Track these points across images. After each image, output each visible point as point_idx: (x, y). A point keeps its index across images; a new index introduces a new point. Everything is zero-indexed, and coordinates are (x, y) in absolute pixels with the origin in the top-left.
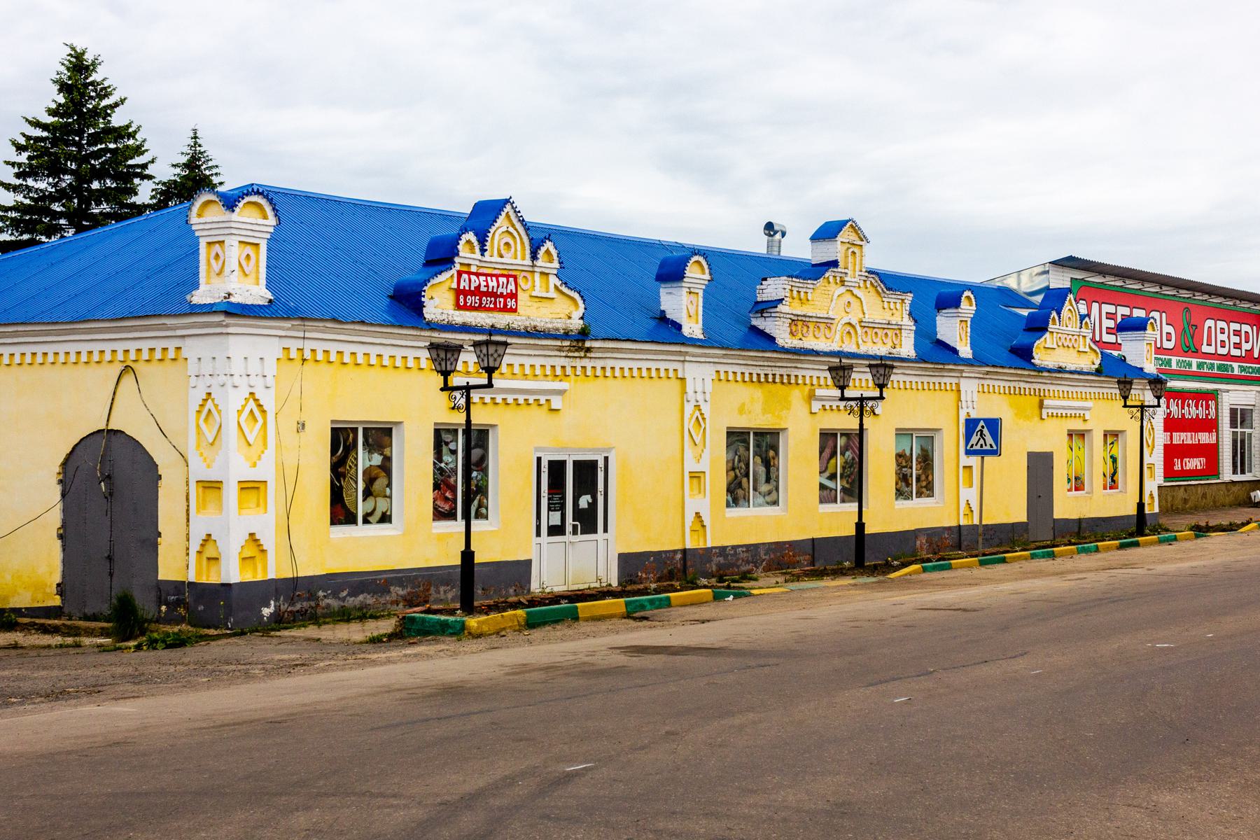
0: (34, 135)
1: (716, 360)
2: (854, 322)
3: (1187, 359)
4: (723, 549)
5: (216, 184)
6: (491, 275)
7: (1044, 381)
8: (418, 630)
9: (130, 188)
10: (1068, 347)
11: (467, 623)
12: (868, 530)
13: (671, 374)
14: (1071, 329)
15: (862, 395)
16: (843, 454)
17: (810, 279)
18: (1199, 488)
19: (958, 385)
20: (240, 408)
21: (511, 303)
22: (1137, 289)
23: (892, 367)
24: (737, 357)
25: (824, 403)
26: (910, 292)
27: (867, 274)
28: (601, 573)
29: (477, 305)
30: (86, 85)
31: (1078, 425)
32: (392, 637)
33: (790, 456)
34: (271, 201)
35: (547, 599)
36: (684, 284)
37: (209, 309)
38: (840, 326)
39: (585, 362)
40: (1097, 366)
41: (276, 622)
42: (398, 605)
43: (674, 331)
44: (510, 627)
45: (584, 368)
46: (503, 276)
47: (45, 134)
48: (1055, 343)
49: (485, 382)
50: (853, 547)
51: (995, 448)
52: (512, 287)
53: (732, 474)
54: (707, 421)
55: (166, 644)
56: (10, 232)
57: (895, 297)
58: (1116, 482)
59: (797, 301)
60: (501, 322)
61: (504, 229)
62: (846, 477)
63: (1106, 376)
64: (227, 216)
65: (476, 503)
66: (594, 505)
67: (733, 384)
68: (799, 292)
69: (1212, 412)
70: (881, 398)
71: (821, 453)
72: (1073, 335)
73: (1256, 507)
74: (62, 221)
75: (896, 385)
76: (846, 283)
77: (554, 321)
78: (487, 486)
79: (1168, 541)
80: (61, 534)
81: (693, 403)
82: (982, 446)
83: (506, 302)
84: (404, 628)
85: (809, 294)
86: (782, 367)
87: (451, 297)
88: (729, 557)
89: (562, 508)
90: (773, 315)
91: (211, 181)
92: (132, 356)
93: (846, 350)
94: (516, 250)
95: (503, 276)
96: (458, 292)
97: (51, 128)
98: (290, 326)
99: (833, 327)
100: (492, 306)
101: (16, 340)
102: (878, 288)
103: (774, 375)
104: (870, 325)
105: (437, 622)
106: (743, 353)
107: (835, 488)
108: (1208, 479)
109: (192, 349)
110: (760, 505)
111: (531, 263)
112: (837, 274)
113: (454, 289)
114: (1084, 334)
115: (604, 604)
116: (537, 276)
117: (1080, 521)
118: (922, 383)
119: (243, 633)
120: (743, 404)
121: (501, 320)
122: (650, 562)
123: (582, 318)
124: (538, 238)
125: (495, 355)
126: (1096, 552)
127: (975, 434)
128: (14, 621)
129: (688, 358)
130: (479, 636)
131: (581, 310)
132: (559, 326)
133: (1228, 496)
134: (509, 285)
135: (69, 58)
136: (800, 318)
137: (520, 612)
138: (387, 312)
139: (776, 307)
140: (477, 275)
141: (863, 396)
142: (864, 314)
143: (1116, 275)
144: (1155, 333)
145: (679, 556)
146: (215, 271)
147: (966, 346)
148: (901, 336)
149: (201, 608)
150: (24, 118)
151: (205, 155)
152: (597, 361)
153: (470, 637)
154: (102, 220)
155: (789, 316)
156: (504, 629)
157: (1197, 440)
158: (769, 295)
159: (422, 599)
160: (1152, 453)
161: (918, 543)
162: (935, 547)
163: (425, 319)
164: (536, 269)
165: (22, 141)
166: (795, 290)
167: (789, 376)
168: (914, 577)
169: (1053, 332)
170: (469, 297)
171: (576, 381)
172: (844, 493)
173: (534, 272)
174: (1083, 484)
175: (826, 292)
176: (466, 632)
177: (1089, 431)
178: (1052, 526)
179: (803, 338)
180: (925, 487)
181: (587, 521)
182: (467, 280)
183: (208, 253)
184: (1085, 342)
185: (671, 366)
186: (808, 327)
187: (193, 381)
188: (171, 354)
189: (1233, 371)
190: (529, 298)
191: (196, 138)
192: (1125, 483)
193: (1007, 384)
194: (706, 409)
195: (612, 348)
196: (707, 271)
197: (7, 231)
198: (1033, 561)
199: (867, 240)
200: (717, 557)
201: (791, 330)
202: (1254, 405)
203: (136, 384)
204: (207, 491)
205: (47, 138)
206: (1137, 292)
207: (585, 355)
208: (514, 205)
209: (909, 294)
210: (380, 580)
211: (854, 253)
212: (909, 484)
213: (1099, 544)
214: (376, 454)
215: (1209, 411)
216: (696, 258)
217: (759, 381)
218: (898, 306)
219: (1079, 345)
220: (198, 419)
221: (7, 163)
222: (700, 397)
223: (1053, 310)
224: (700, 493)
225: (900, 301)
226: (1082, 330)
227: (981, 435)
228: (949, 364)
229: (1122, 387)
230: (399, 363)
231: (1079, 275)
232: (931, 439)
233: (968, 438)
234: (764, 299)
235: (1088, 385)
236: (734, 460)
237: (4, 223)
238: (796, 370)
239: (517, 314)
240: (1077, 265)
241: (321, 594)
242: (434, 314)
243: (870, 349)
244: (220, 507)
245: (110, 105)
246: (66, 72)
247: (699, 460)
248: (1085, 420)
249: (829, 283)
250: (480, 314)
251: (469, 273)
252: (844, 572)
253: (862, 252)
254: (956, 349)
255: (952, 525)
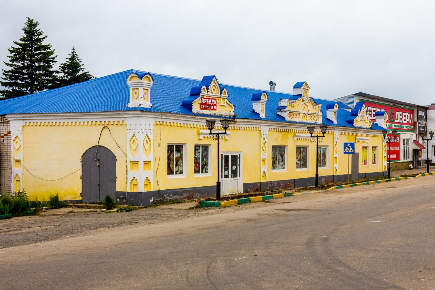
0: (16, 47)
1: (269, 125)
2: (306, 113)
3: (391, 124)
4: (271, 182)
5: (81, 65)
8: (205, 205)
9: (50, 66)
11: (221, 203)
12: (319, 176)
13: (257, 129)
16: (302, 153)
17: (294, 100)
19: (333, 132)
20: (144, 139)
21: (215, 107)
22: (378, 102)
25: (298, 138)
26: (321, 104)
27: (309, 98)
28: (238, 189)
29: (206, 108)
30: (34, 31)
31: (365, 145)
34: (152, 76)
36: (260, 102)
37: (135, 109)
38: (302, 114)
39: (235, 126)
40: (371, 126)
41: (154, 204)
42: (185, 199)
43: (257, 116)
45: (234, 127)
46: (213, 99)
47: (20, 47)
48: (359, 119)
49: (224, 132)
50: (216, 188)
51: (353, 151)
52: (215, 102)
55: (126, 210)
56: (8, 80)
57: (317, 105)
59: (291, 106)
61: (213, 85)
64: (140, 81)
66: (236, 169)
68: (291, 104)
69: (398, 140)
70: (324, 136)
73: (411, 170)
74: (26, 76)
76: (304, 101)
77: (226, 113)
80: (82, 178)
81: (263, 138)
82: (349, 151)
83: (213, 107)
84: (200, 205)
85: (294, 104)
87: (199, 105)
88: (273, 185)
89: (228, 170)
90: (284, 111)
91: (79, 64)
92: (107, 123)
93: (304, 121)
94: (216, 91)
95: (213, 99)
96: (201, 104)
97: (23, 45)
98: (157, 114)
99: (300, 114)
100: (210, 108)
101: (66, 118)
103: (284, 129)
104: (310, 114)
107: (300, 163)
108: (397, 161)
109: (128, 121)
110: (280, 169)
113: (200, 103)
114: (367, 117)
115: (257, 198)
116: (222, 99)
117: (366, 174)
119: (146, 207)
121: (213, 112)
123: (234, 112)
124: (222, 88)
125: (227, 124)
126: (380, 183)
127: (347, 147)
128: (67, 205)
129: (262, 124)
130: (225, 207)
131: (233, 110)
135: (28, 22)
136: (291, 112)
137: (236, 200)
138: (180, 109)
139: (285, 108)
141: (219, 132)
142: (308, 110)
144: (386, 116)
145: (259, 184)
146: (135, 98)
147: (335, 120)
149: (132, 200)
150: (13, 41)
151: (77, 55)
152: (238, 125)
153: (222, 207)
154: (40, 76)
155: (288, 111)
156: (232, 205)
163: (192, 112)
164: (222, 97)
165: (12, 49)
166: (290, 103)
167: (288, 129)
168: (334, 190)
170: (204, 105)
174: (366, 162)
176: (221, 206)
177: (368, 146)
179: (292, 118)
181: (235, 173)
182: (203, 100)
183: (133, 92)
184: (368, 119)
185: (257, 126)
186: (294, 114)
187: (128, 131)
188: (121, 123)
189: (404, 128)
191: (74, 50)
195: (242, 121)
196: (267, 97)
197: (8, 79)
201: (289, 115)
202: (410, 138)
203: (109, 132)
204: (133, 164)
205: (20, 48)
206: (377, 103)
207: (235, 123)
209: (321, 104)
210: (181, 191)
211: (306, 92)
213: (380, 180)
216: (264, 94)
217: (280, 131)
218: (318, 108)
220: (130, 143)
221: (8, 56)
223: (359, 109)
226: (367, 115)
227: (349, 148)
228: (331, 126)
229: (384, 133)
230: (185, 126)
231: (362, 98)
234: (281, 106)
236: (273, 155)
237: (6, 76)
241: (165, 195)
243: (310, 122)
244: (138, 169)
245: (42, 38)
246: (27, 27)
248: (367, 143)
249: (299, 101)
251: (204, 98)
252: (313, 189)
253: (308, 91)
255: (331, 175)
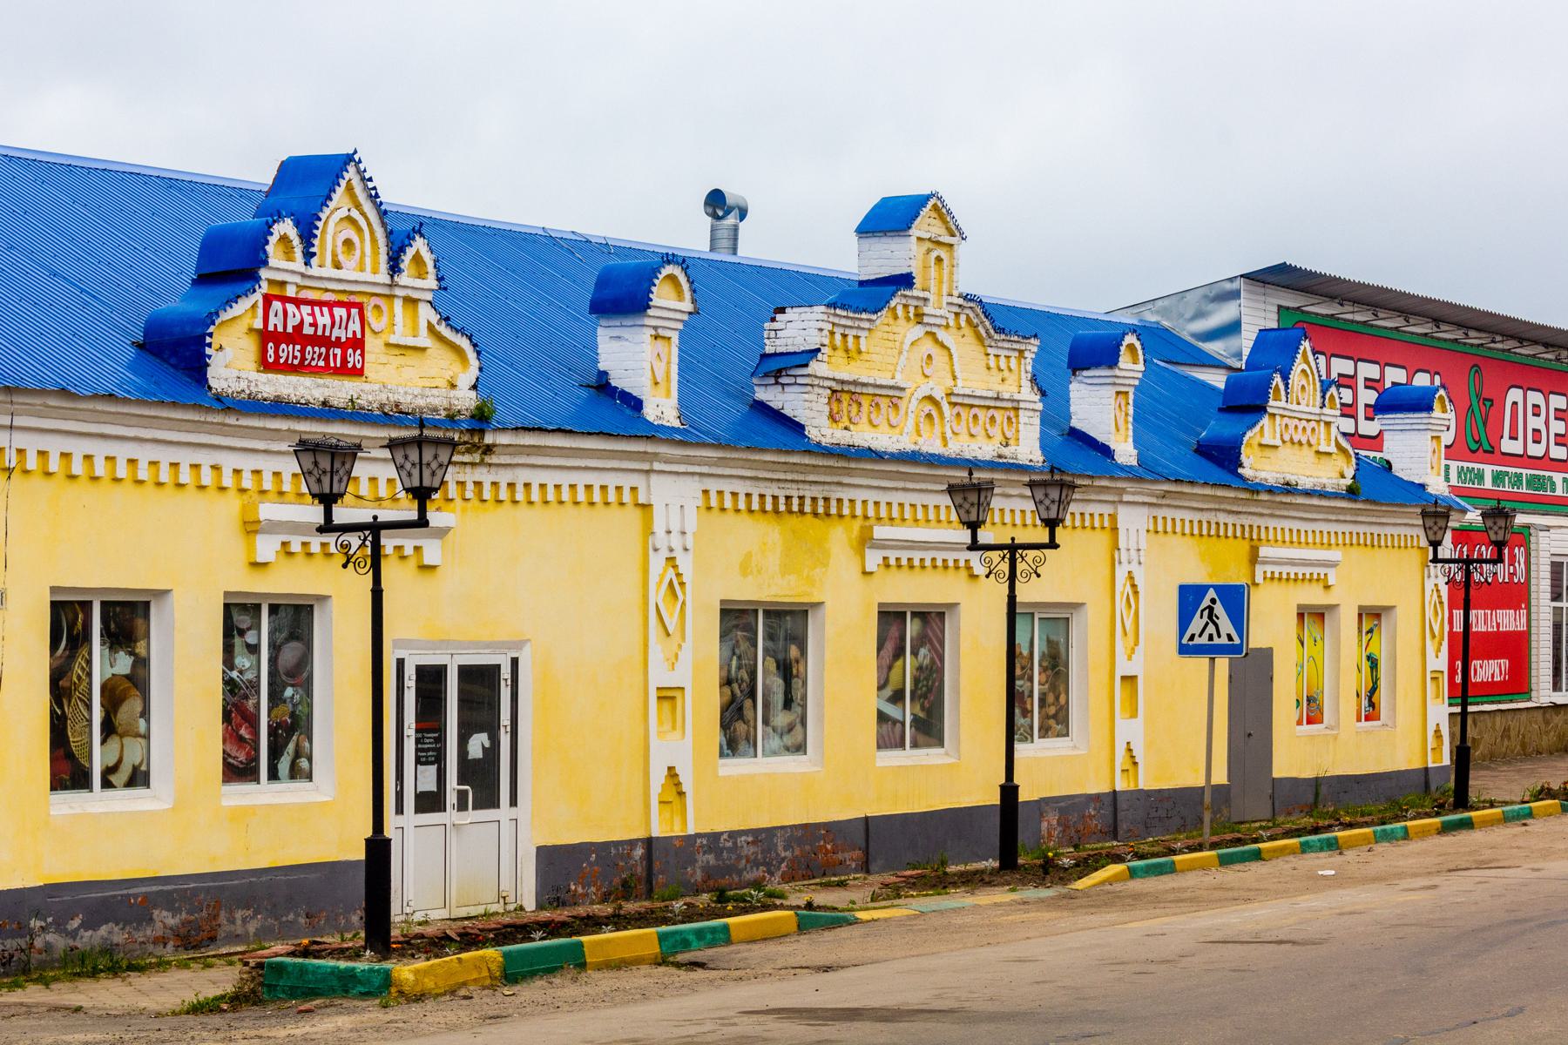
1: (705, 469)
2: (939, 394)
3: (1476, 466)
4: (714, 837)
6: (321, 304)
7: (1259, 510)
8: (292, 988)
10: (1300, 443)
11: (395, 974)
12: (1023, 796)
13: (627, 497)
14: (1307, 409)
15: (1013, 539)
16: (915, 653)
17: (865, 311)
18: (1498, 719)
19: (1113, 517)
21: (353, 358)
23: (1073, 487)
24: (741, 463)
27: (961, 301)
28: (507, 885)
29: (296, 362)
31: (1313, 596)
32: (238, 1000)
33: (828, 656)
35: (490, 930)
39: (482, 474)
40: (1349, 482)
42: (165, 945)
43: (628, 412)
44: (475, 980)
45: (478, 484)
46: (340, 304)
49: (413, 515)
51: (1237, 641)
52: (355, 326)
53: (727, 690)
54: (688, 587)
58: (1376, 706)
59: (840, 353)
60: (339, 395)
61: (343, 213)
62: (920, 697)
63: (1367, 501)
65: (291, 747)
66: (492, 752)
67: (731, 515)
68: (844, 336)
70: (1052, 545)
71: (879, 649)
72: (1308, 421)
75: (997, 519)
76: (926, 320)
77: (427, 392)
78: (310, 717)
79: (1518, 819)
81: (665, 553)
82: (1211, 638)
86: (816, 482)
87: (250, 346)
88: (725, 854)
89: (439, 760)
90: (800, 380)
95: (340, 304)
96: (266, 336)
99: (903, 405)
100: (321, 363)
102: (981, 329)
103: (801, 498)
104: (967, 401)
105: (332, 973)
106: (757, 457)
107: (901, 719)
108: (1511, 701)
110: (774, 753)
111: (387, 280)
112: (910, 302)
113: (257, 331)
116: (398, 305)
117: (1317, 782)
118: (889, 504)
120: (749, 555)
121: (339, 390)
122: (591, 864)
123: (474, 387)
125: (434, 465)
126: (1405, 839)
127: (1199, 612)
129: (657, 466)
130: (420, 998)
131: (472, 373)
132: (436, 402)
133: (1547, 733)
134: (351, 322)
136: (846, 388)
139: (806, 365)
140: (298, 302)
142: (955, 378)
143: (1355, 302)
145: (639, 852)
148: (1018, 423)
156: (464, 984)
157: (1495, 624)
158: (790, 341)
159: (204, 935)
160: (1133, 651)
161: (1044, 825)
162: (1073, 834)
163: (210, 388)
164: (398, 292)
166: (839, 331)
167: (826, 499)
168: (1118, 887)
169: (1274, 415)
171: (464, 510)
172: (917, 729)
173: (394, 296)
175: (891, 337)
176: (393, 990)
178: (1270, 791)
179: (852, 427)
180: (1055, 716)
185: (627, 481)
189: (1553, 490)
190: (383, 348)
192: (1393, 708)
193: (1196, 516)
194: (685, 563)
196: (687, 294)
198: (1305, 856)
199: (961, 234)
200: (705, 853)
207: (482, 460)
208: (362, 167)
209: (1032, 341)
210: (135, 896)
211: (939, 260)
212: (1028, 712)
213: (1409, 824)
214: (122, 653)
215: (1515, 568)
216: (669, 270)
217: (776, 511)
219: (1319, 439)
222: (675, 540)
224: (674, 728)
225: (1016, 354)
227: (1210, 617)
231: (1291, 300)
232: (1062, 625)
233: (1184, 621)
234: (779, 350)
235: (1334, 518)
238: (840, 489)
239: (364, 379)
240: (1289, 283)
241: (35, 924)
242: (226, 379)
243: (965, 448)
247: (673, 664)
248: (1327, 587)
250: (302, 379)
251: (285, 300)
253: (952, 257)
254: (1108, 447)
